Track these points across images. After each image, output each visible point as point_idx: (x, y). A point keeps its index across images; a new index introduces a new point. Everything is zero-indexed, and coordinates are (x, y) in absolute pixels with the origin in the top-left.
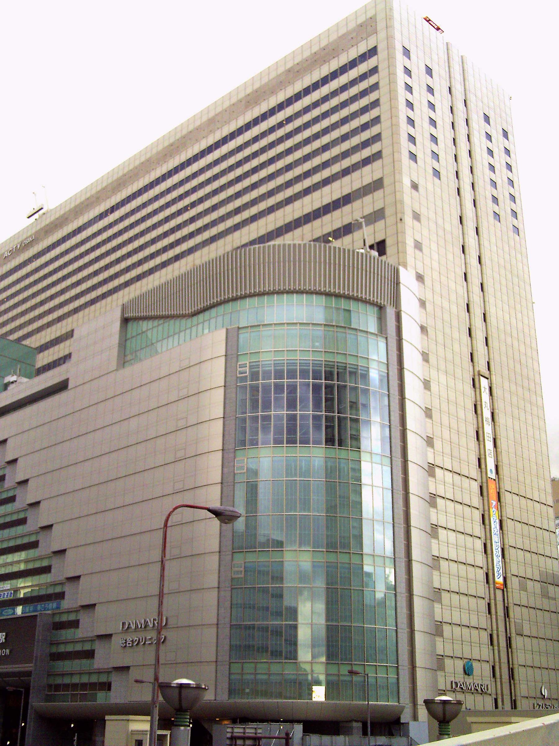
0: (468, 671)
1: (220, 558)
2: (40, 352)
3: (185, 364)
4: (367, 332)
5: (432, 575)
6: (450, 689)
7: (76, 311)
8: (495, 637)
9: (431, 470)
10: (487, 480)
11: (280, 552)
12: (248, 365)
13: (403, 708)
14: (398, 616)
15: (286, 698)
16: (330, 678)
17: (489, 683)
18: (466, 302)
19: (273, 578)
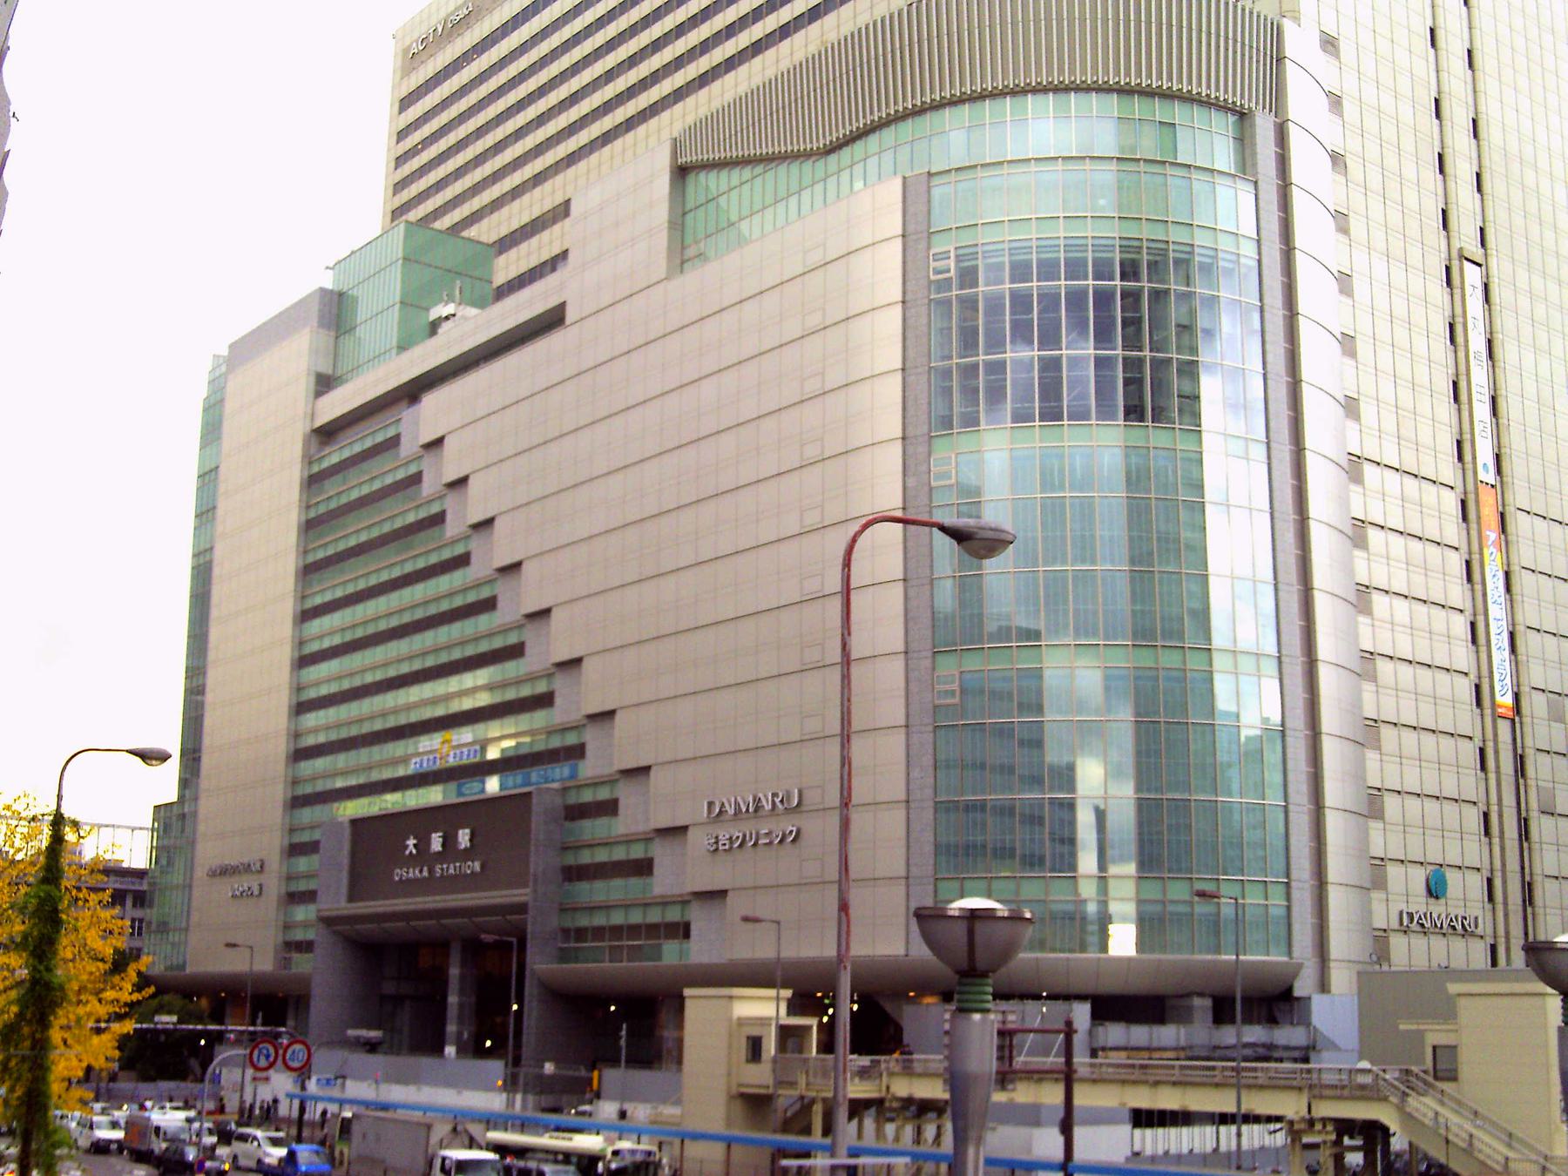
2: (500, 253)
3: (816, 258)
4: (1212, 171)
5: (1360, 691)
7: (572, 159)
8: (1498, 883)
9: (1354, 467)
10: (1476, 489)
11: (1035, 651)
12: (952, 255)
13: (1300, 966)
14: (1291, 831)
15: (1053, 950)
16: (1150, 908)
17: (1479, 913)
18: (1434, 94)
19: (1020, 705)
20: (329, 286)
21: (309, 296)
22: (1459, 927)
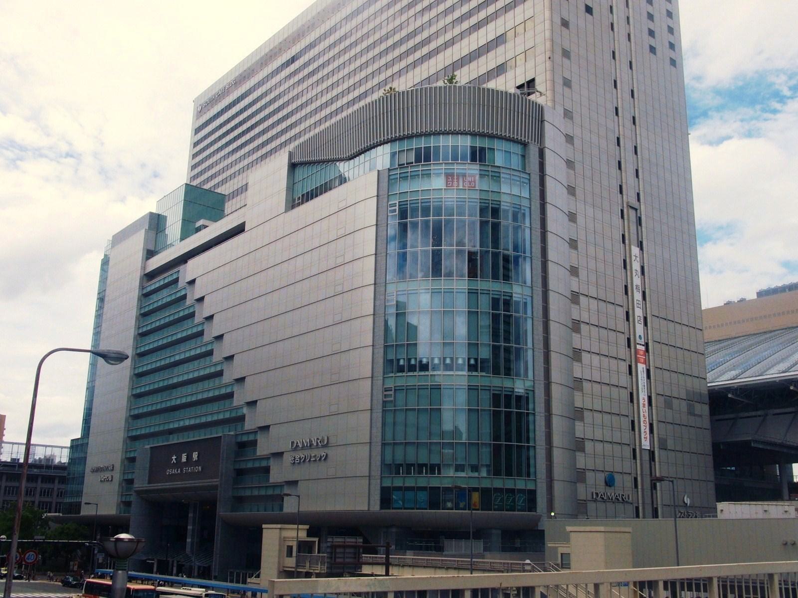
1: (372, 383)
12: (397, 205)
20: (154, 211)
21: (143, 217)
22: (621, 499)
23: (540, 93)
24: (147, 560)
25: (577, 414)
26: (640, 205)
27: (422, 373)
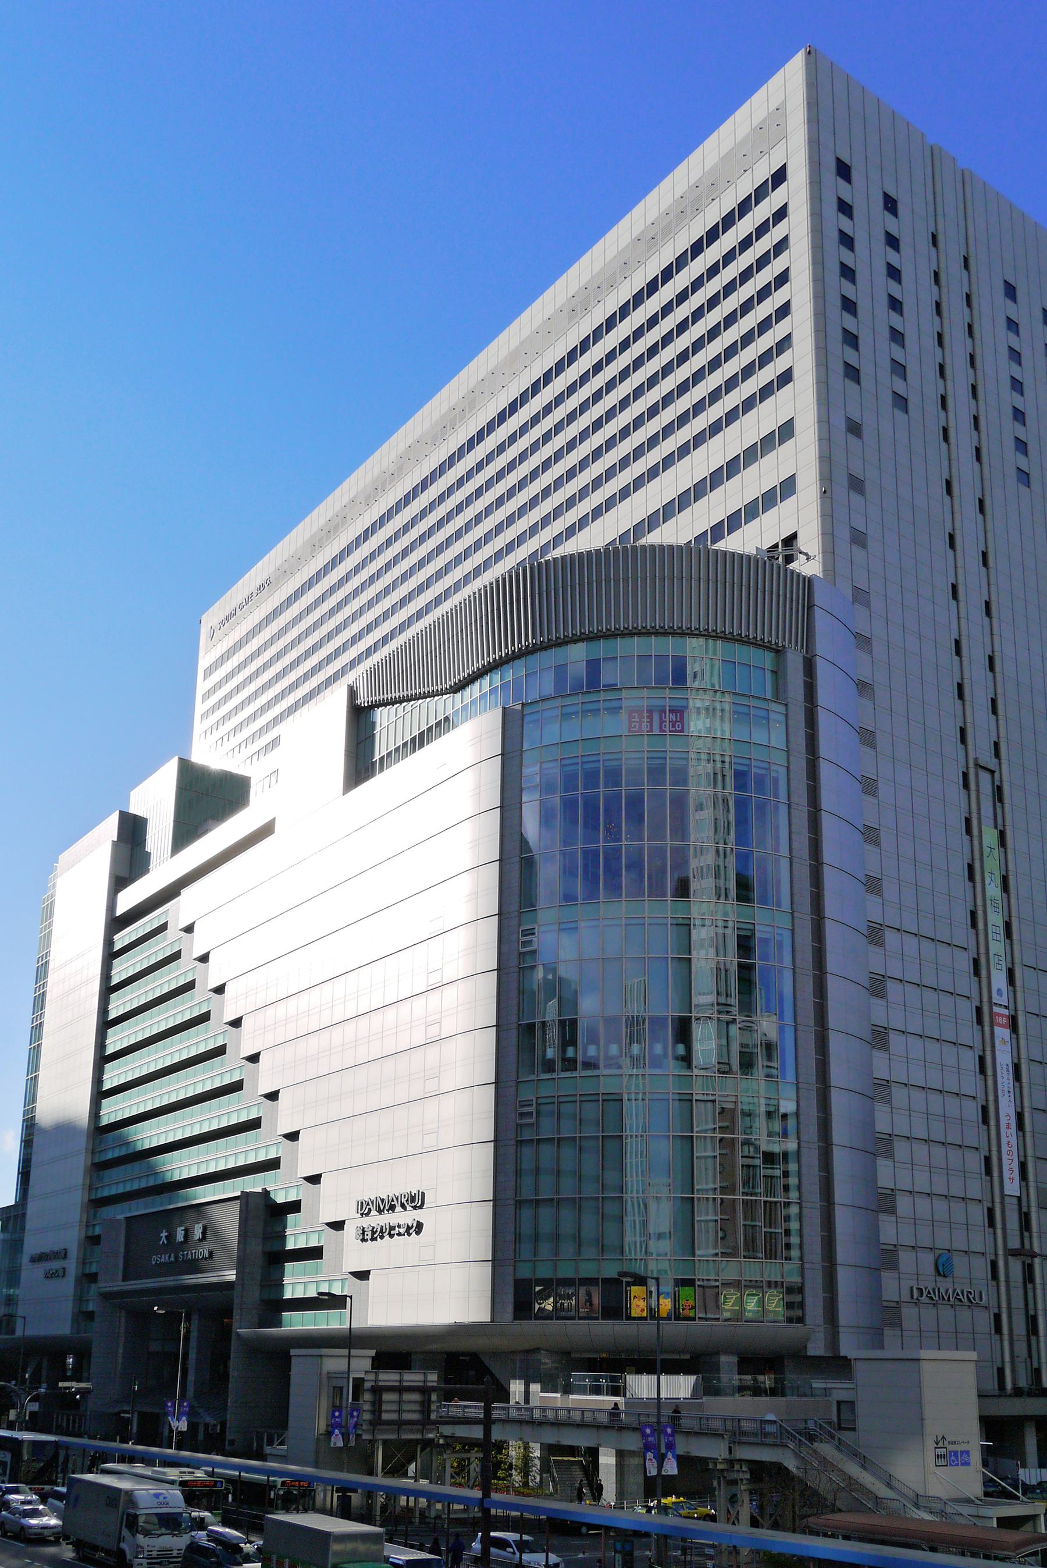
0: (941, 1270)
5: (873, 1111)
6: (907, 1298)
8: (983, 960)
23: (806, 554)
24: (120, 1413)
25: (881, 1146)
26: (1000, 764)
27: (589, 1073)
